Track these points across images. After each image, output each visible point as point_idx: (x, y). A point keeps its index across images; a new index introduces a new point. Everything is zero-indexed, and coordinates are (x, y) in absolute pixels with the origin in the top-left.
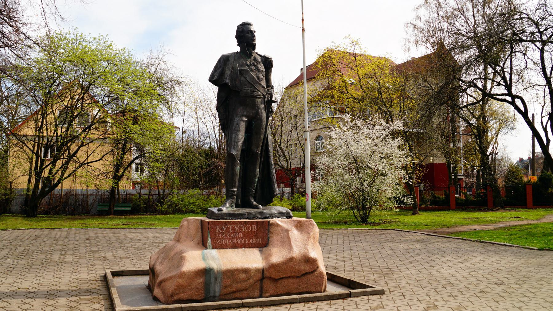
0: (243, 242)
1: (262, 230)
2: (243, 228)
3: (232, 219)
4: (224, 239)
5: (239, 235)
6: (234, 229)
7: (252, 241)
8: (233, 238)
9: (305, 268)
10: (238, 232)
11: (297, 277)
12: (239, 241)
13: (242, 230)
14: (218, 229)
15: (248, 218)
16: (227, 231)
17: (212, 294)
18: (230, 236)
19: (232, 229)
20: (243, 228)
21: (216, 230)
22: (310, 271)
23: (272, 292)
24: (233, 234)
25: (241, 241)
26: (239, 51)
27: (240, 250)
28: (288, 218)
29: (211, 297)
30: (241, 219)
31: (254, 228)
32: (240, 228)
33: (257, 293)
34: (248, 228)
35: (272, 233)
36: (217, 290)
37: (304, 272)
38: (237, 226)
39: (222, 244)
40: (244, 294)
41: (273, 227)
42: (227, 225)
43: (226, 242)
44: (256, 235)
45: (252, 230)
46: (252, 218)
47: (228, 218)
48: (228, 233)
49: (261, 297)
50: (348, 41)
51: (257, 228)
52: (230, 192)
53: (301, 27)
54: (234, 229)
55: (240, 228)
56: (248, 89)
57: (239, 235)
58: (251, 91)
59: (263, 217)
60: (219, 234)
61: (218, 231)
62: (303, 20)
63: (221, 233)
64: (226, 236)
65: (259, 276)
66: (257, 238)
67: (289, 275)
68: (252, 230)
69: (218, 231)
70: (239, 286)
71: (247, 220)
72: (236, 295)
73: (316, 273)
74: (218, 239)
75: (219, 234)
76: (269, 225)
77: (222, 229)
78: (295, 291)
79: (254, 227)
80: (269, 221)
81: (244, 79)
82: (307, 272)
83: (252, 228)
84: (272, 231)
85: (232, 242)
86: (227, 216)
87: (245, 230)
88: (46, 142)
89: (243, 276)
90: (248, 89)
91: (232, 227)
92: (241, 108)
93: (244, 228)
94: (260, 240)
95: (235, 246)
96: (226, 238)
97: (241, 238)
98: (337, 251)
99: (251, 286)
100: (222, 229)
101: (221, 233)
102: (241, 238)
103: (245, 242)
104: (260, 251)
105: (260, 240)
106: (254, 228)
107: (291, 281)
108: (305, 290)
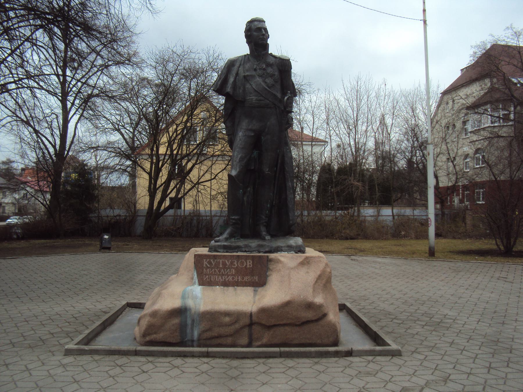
0: (236, 279)
1: (260, 266)
2: (235, 263)
3: (227, 252)
4: (213, 275)
5: (230, 271)
6: (224, 264)
7: (246, 279)
8: (223, 275)
9: (309, 315)
10: (229, 268)
11: (296, 325)
12: (230, 278)
13: (235, 265)
14: (205, 263)
15: (245, 251)
16: (217, 265)
17: (189, 337)
18: (219, 271)
19: (222, 264)
20: (235, 263)
21: (203, 264)
22: (314, 319)
23: (265, 341)
24: (224, 270)
25: (233, 278)
26: (249, 53)
27: (231, 289)
28: (296, 253)
29: (188, 340)
30: (237, 252)
31: (249, 264)
32: (232, 263)
33: (245, 340)
34: (242, 263)
35: (272, 270)
36: (196, 334)
37: (304, 320)
38: (228, 261)
39: (211, 280)
40: (229, 340)
41: (273, 263)
42: (216, 259)
43: (215, 279)
44: (251, 272)
45: (246, 266)
46: (251, 252)
47: (222, 250)
48: (217, 268)
49: (249, 345)
50: (509, 33)
51: (253, 263)
52: (231, 221)
53: (422, 18)
54: (224, 264)
55: (232, 263)
56: (253, 97)
57: (230, 271)
58: (256, 100)
59: (264, 251)
60: (206, 269)
61: (206, 265)
62: (424, 11)
63: (209, 268)
64: (215, 271)
65: (247, 321)
66: (253, 276)
67: (285, 322)
68: (246, 266)
69: (206, 265)
70: (223, 331)
71: (245, 254)
72: (219, 341)
73: (322, 322)
74: (206, 275)
75: (206, 269)
76: (267, 260)
77: (210, 263)
78: (296, 342)
79: (250, 262)
80: (268, 256)
81: (250, 87)
82: (309, 319)
83: (246, 263)
84: (271, 268)
85: (222, 279)
86: (221, 248)
87: (238, 265)
88: (49, 156)
89: (227, 319)
90: (253, 97)
91: (222, 261)
92: (247, 121)
93: (237, 263)
94: (256, 278)
95: (226, 284)
96: (215, 275)
97: (232, 275)
98: (516, 273)
99: (237, 332)
100: (210, 263)
101: (209, 268)
102: (232, 275)
103: (238, 280)
104: (254, 291)
105: (256, 278)
106: (249, 264)
107: (288, 328)
108: (308, 341)
